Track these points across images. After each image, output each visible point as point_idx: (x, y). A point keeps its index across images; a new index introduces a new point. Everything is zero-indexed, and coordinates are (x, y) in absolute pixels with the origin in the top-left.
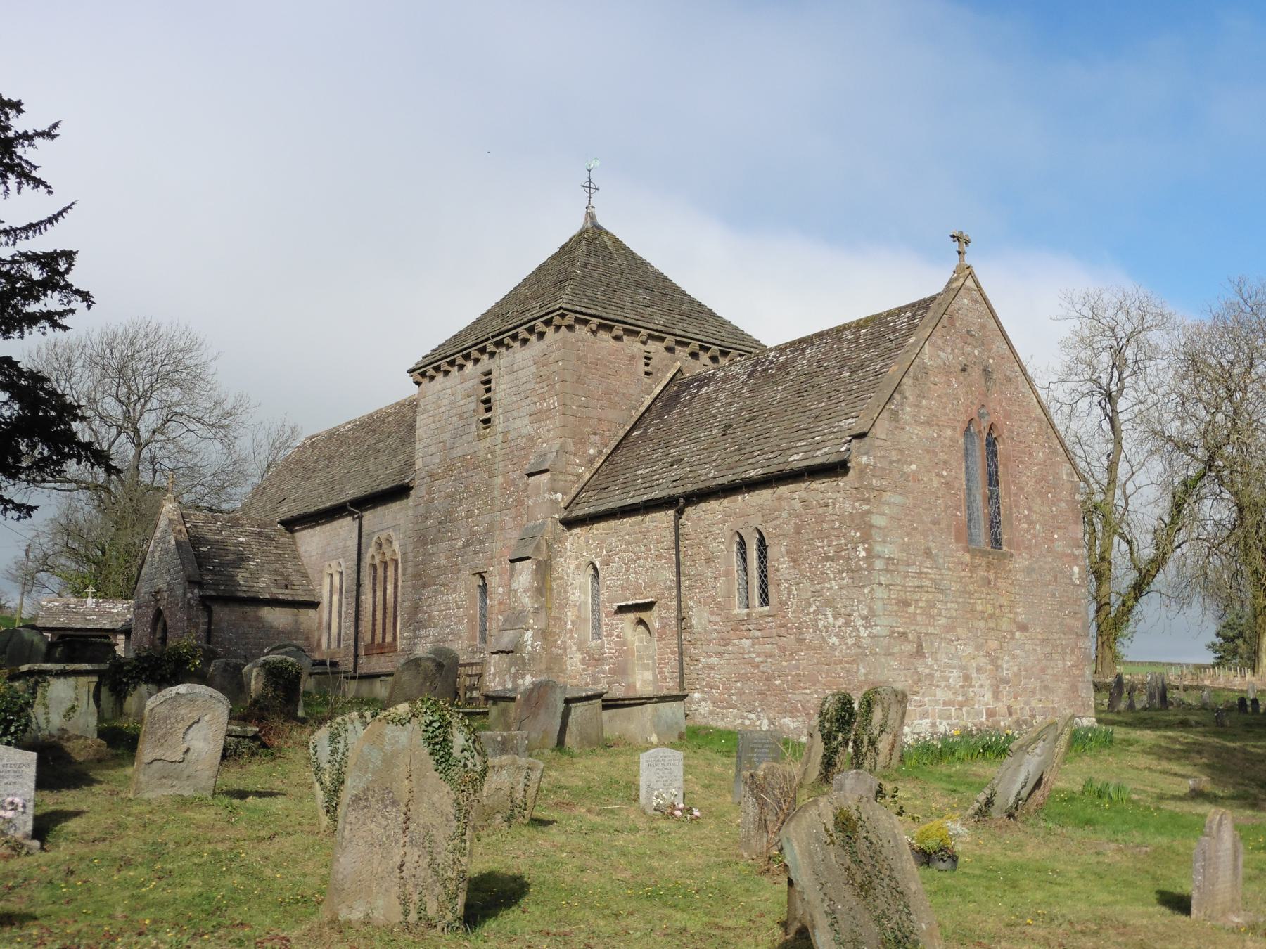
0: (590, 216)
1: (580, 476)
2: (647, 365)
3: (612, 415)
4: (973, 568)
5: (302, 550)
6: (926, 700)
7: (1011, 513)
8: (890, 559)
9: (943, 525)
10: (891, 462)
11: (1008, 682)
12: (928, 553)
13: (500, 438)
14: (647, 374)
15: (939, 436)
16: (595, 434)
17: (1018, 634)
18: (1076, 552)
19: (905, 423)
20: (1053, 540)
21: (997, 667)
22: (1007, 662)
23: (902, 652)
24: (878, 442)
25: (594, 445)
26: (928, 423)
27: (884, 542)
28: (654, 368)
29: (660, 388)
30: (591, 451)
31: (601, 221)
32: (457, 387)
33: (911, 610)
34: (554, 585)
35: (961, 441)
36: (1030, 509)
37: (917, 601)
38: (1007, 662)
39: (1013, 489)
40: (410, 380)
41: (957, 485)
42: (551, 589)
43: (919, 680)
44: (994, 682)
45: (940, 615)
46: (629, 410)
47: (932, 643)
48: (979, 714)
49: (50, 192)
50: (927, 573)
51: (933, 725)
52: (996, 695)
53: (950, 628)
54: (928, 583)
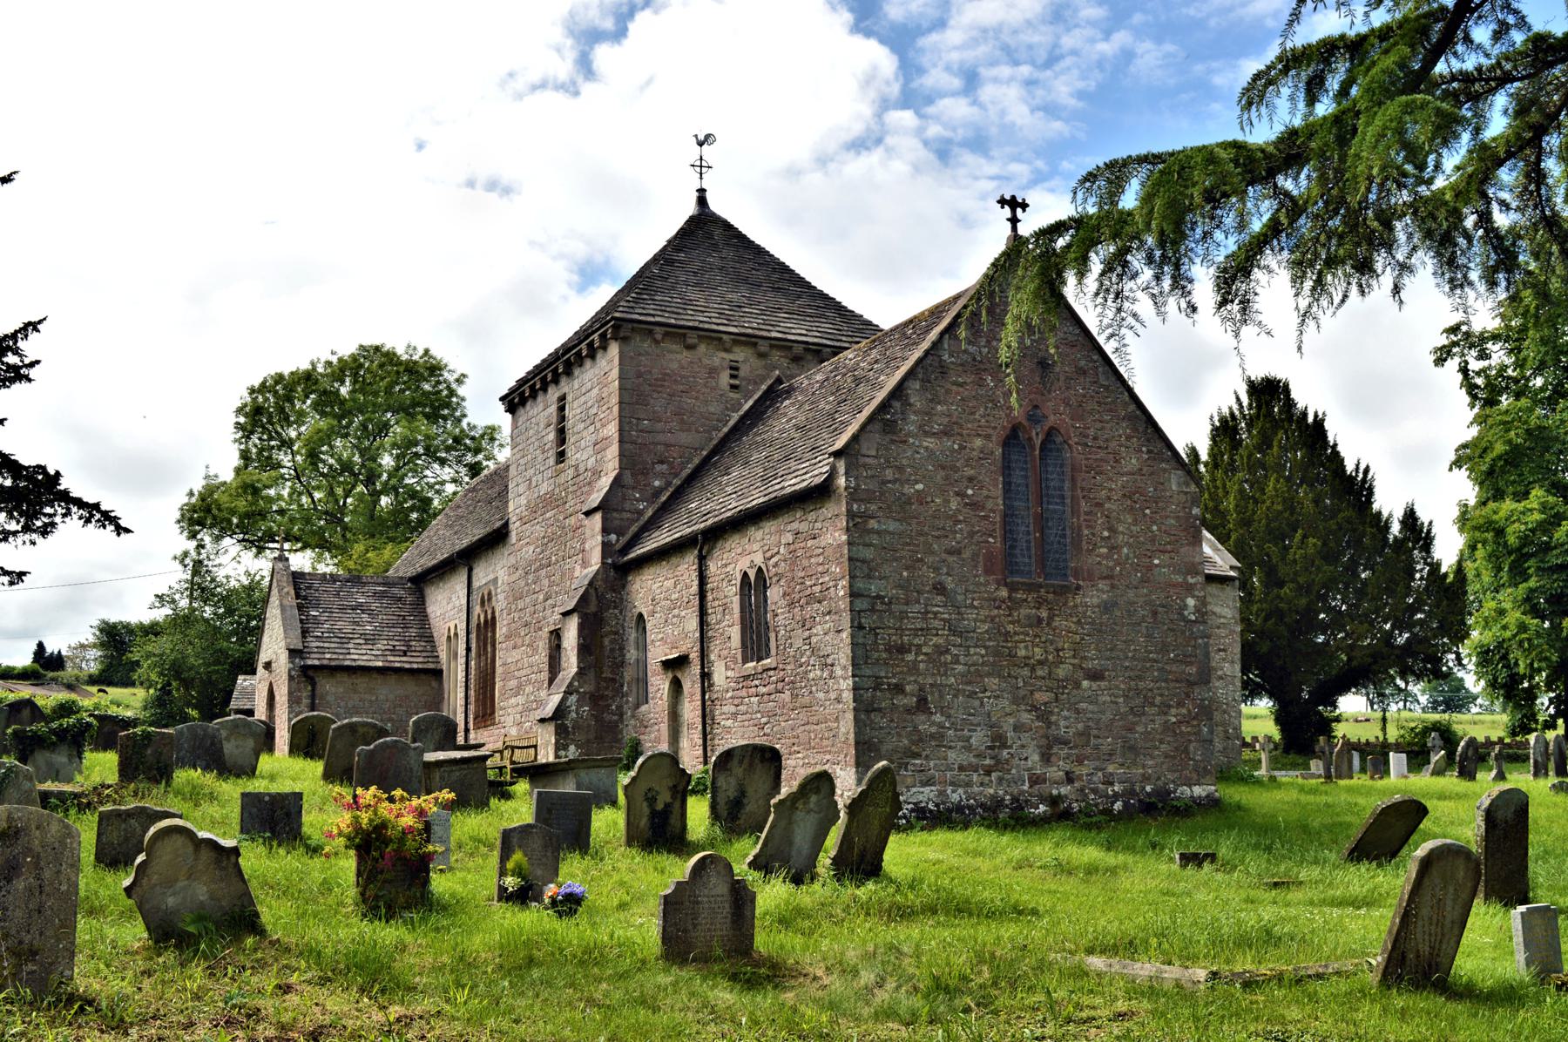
0: (702, 200)
1: (640, 513)
2: (733, 377)
3: (685, 438)
4: (1013, 605)
5: (429, 610)
6: (932, 764)
7: (1080, 535)
8: (878, 597)
9: (967, 554)
10: (884, 483)
11: (1066, 743)
12: (940, 589)
13: (571, 472)
14: (733, 387)
15: (962, 448)
16: (662, 462)
17: (1085, 683)
18: (1191, 581)
19: (909, 434)
20: (1151, 567)
21: (1049, 724)
22: (1066, 718)
23: (894, 707)
24: (862, 460)
25: (661, 475)
26: (946, 433)
27: (869, 577)
28: (744, 379)
29: (750, 403)
30: (657, 483)
31: (716, 206)
32: (542, 411)
33: (910, 657)
34: (606, 641)
35: (999, 451)
36: (1111, 529)
37: (919, 646)
38: (1066, 718)
39: (1084, 506)
40: (501, 407)
41: (990, 504)
42: (602, 647)
43: (921, 740)
44: (1044, 742)
45: (957, 662)
46: (709, 432)
47: (941, 697)
48: (1018, 781)
49: (471, 184)
50: (935, 614)
51: (942, 793)
52: (1046, 758)
53: (973, 676)
54: (936, 623)
